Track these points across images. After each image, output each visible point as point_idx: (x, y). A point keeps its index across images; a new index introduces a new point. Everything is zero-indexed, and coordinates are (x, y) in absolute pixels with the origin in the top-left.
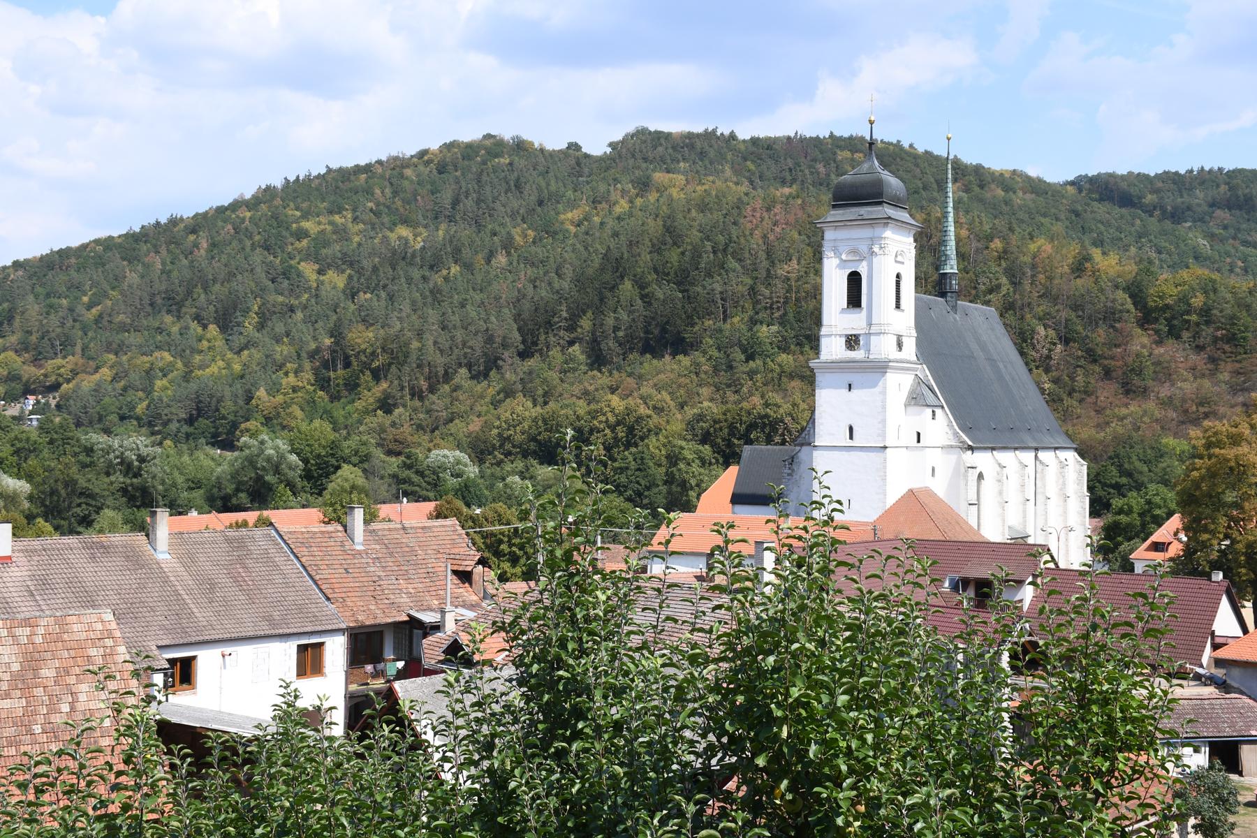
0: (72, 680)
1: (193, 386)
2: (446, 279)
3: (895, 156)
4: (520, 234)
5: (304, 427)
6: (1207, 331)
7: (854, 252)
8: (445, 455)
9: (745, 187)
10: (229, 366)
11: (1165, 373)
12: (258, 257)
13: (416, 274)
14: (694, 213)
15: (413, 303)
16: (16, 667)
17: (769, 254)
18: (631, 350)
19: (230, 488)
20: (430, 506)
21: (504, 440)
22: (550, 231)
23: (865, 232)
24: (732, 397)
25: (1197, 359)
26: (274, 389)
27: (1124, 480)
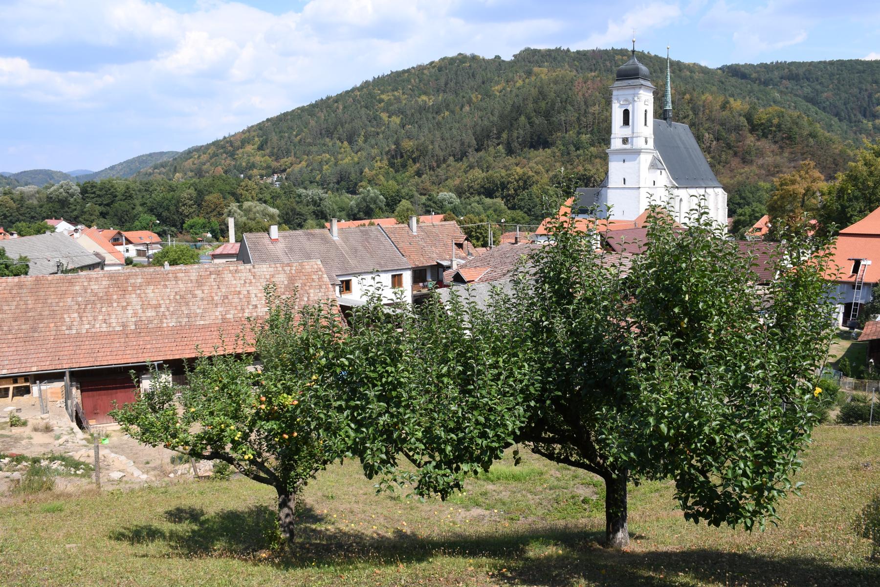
0: (307, 288)
1: (339, 168)
2: (443, 118)
3: (643, 57)
4: (475, 97)
5: (385, 183)
6: (779, 135)
7: (626, 100)
8: (445, 195)
9: (574, 73)
10: (353, 159)
11: (761, 154)
12: (363, 111)
13: (430, 116)
14: (552, 85)
15: (429, 128)
16: (286, 283)
17: (585, 103)
18: (525, 147)
19: (356, 211)
20: (442, 216)
21: (470, 187)
22: (488, 95)
23: (631, 91)
24: (570, 167)
25: (775, 147)
26: (372, 168)
27: (742, 201)
